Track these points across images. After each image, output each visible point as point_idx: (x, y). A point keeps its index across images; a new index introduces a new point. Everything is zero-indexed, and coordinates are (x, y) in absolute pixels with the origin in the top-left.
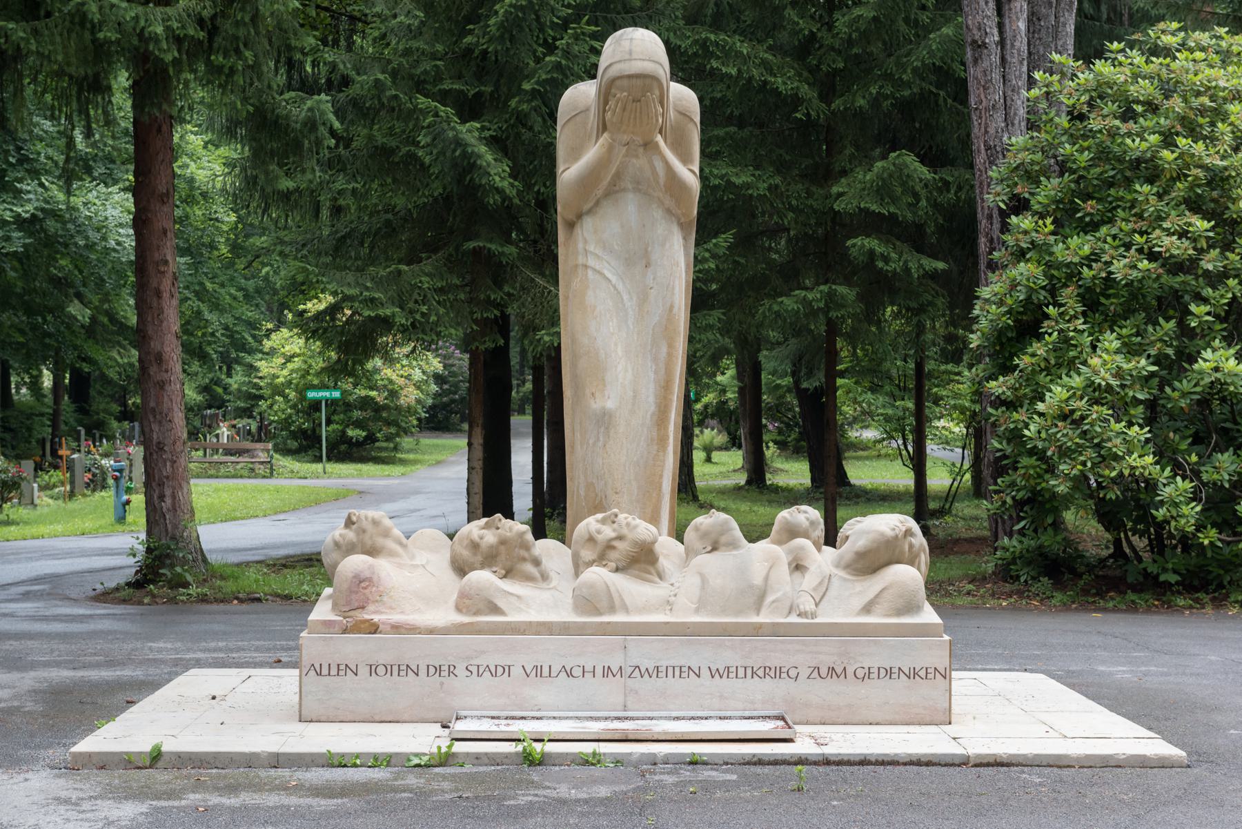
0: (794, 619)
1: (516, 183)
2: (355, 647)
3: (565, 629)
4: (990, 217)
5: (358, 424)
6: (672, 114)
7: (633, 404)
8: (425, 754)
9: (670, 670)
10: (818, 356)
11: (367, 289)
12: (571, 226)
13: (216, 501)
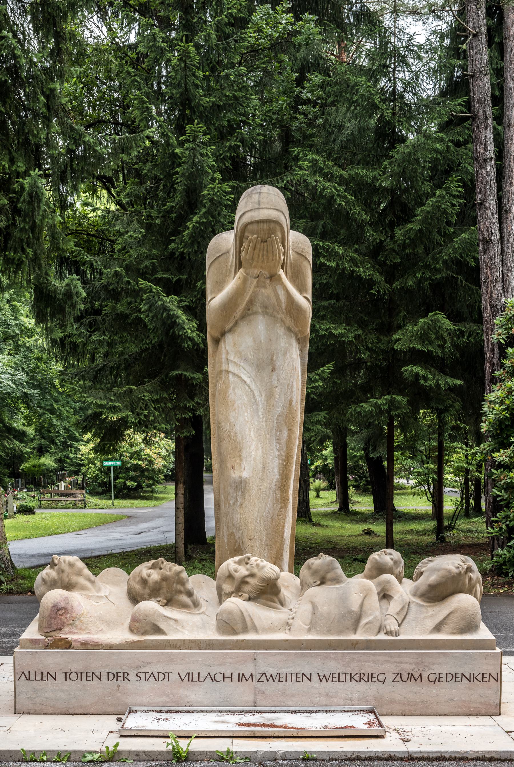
0: (382, 637)
1: (201, 335)
2: (53, 659)
3: (210, 645)
4: (492, 350)
5: (132, 479)
6: (291, 254)
7: (263, 474)
8: (97, 752)
9: (289, 676)
10: (378, 439)
11: (111, 401)
12: (217, 341)
13: (50, 523)
